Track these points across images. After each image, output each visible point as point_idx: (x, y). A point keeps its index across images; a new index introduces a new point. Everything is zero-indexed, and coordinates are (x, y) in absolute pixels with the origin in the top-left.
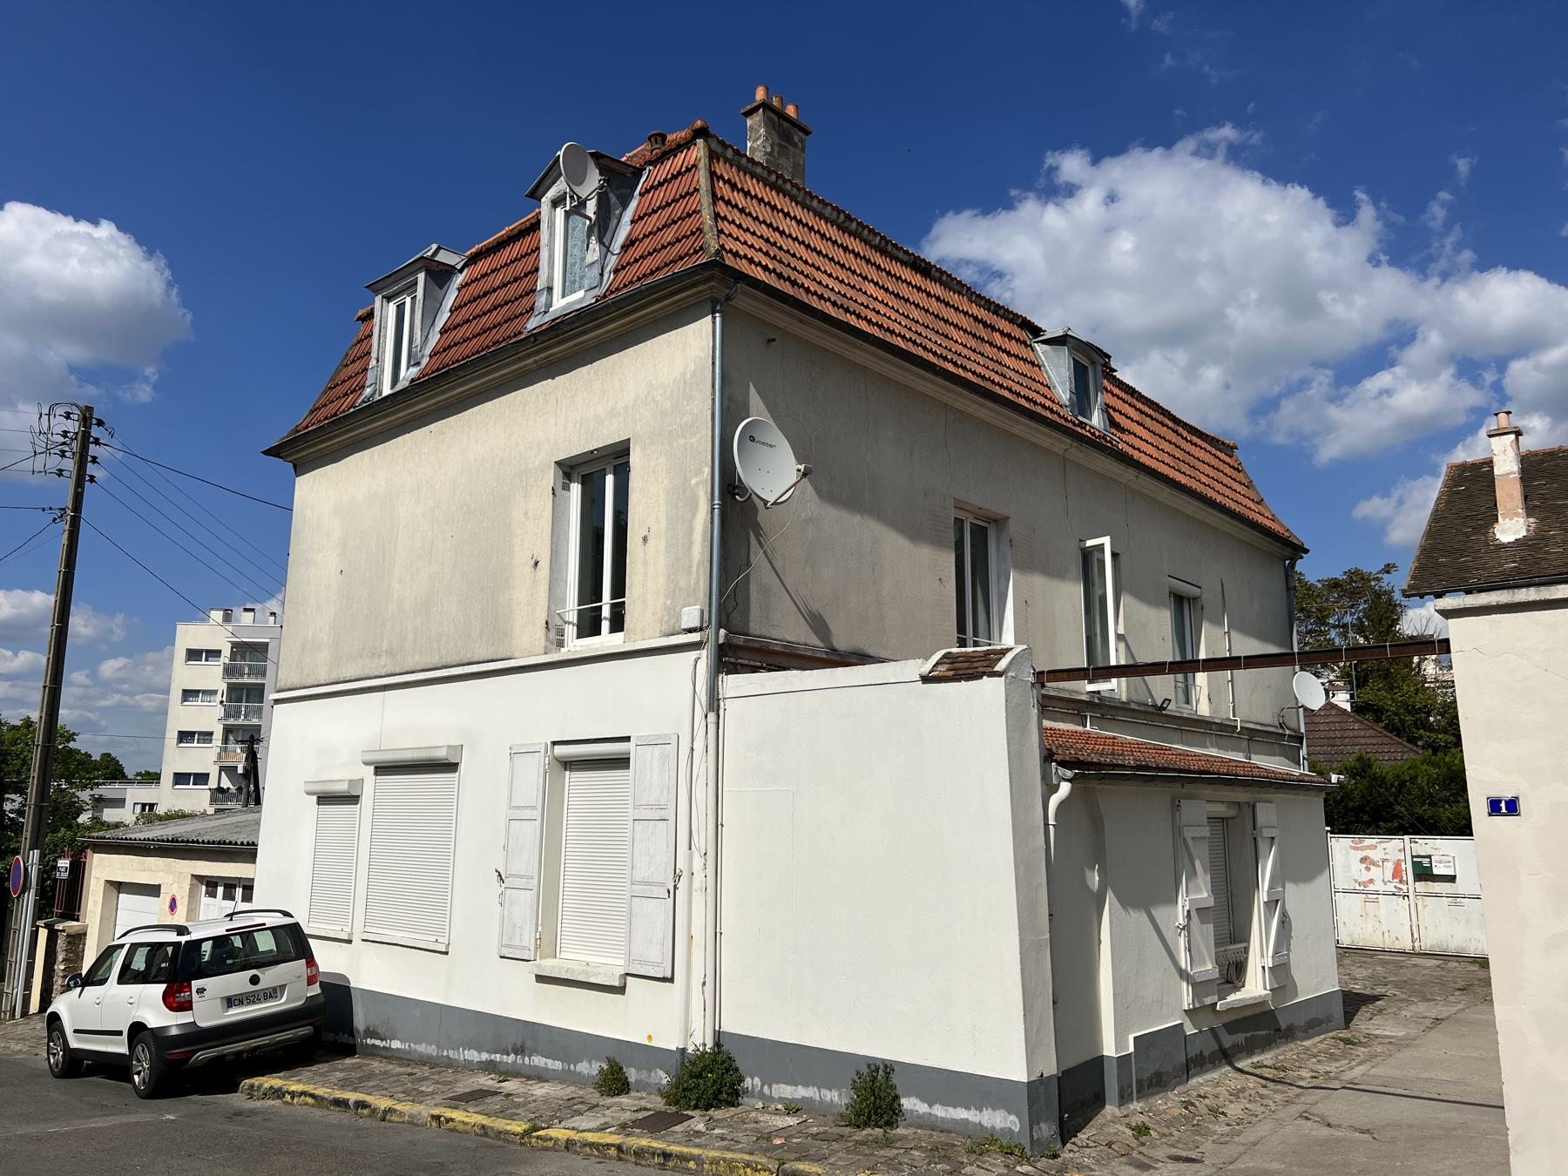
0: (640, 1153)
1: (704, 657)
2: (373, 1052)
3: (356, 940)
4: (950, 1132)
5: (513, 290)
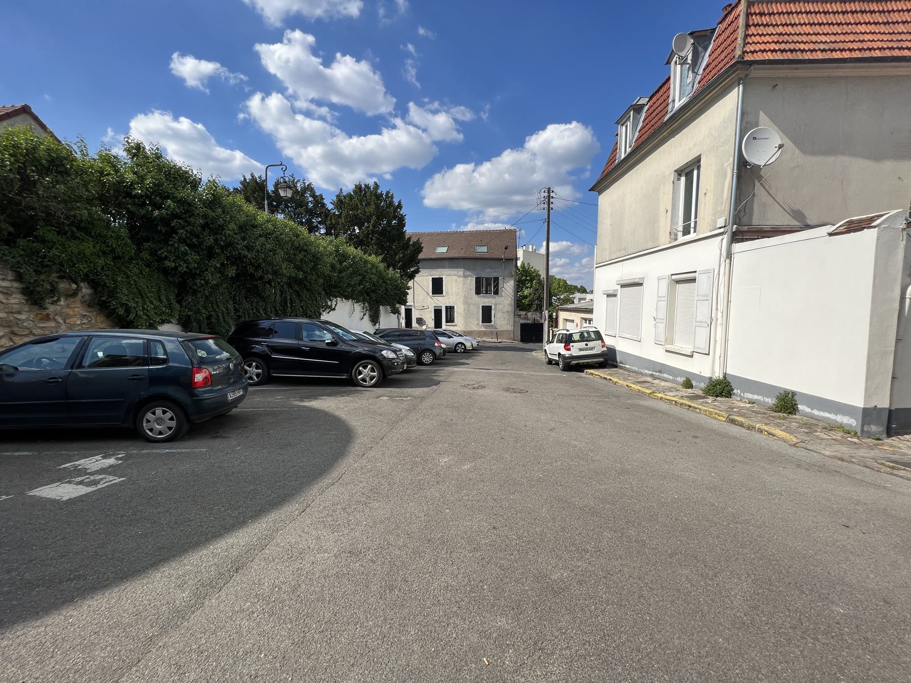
0: (682, 404)
1: (726, 238)
2: (622, 368)
3: (617, 336)
4: (820, 420)
5: (663, 106)
